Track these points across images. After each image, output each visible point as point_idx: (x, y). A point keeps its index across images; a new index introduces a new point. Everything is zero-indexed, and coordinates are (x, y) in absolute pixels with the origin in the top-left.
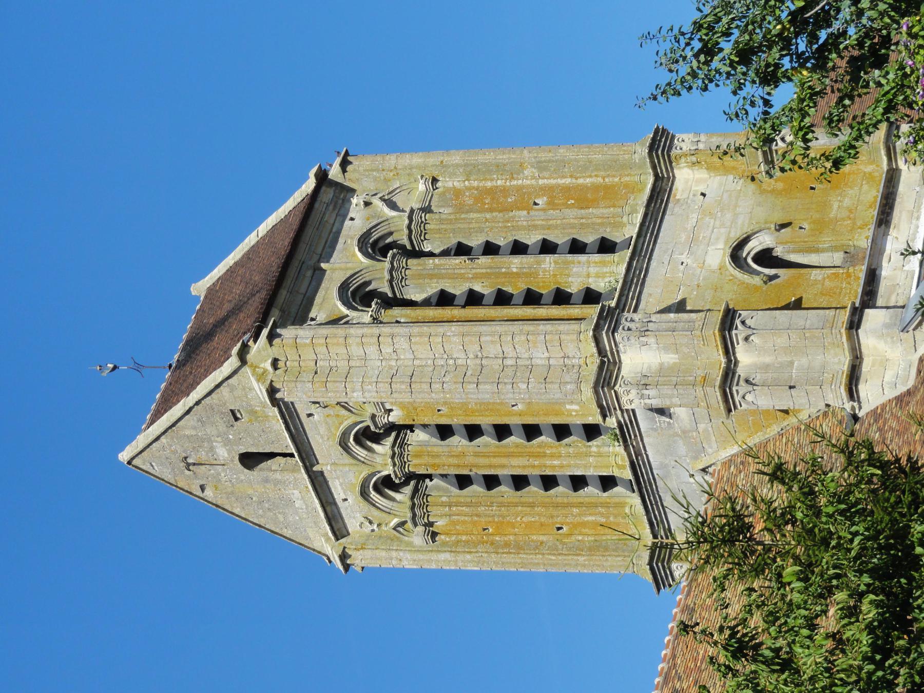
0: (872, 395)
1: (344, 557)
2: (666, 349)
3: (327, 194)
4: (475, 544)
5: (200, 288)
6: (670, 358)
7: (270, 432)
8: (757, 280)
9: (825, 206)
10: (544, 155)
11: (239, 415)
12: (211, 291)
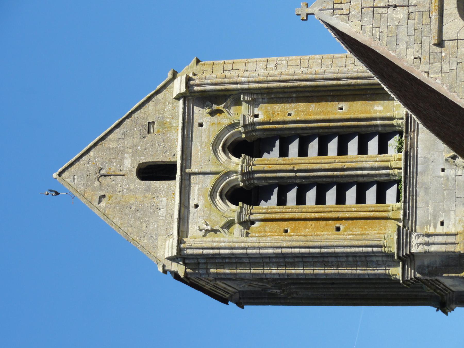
7: (168, 141)
10: (383, 249)
11: (152, 130)
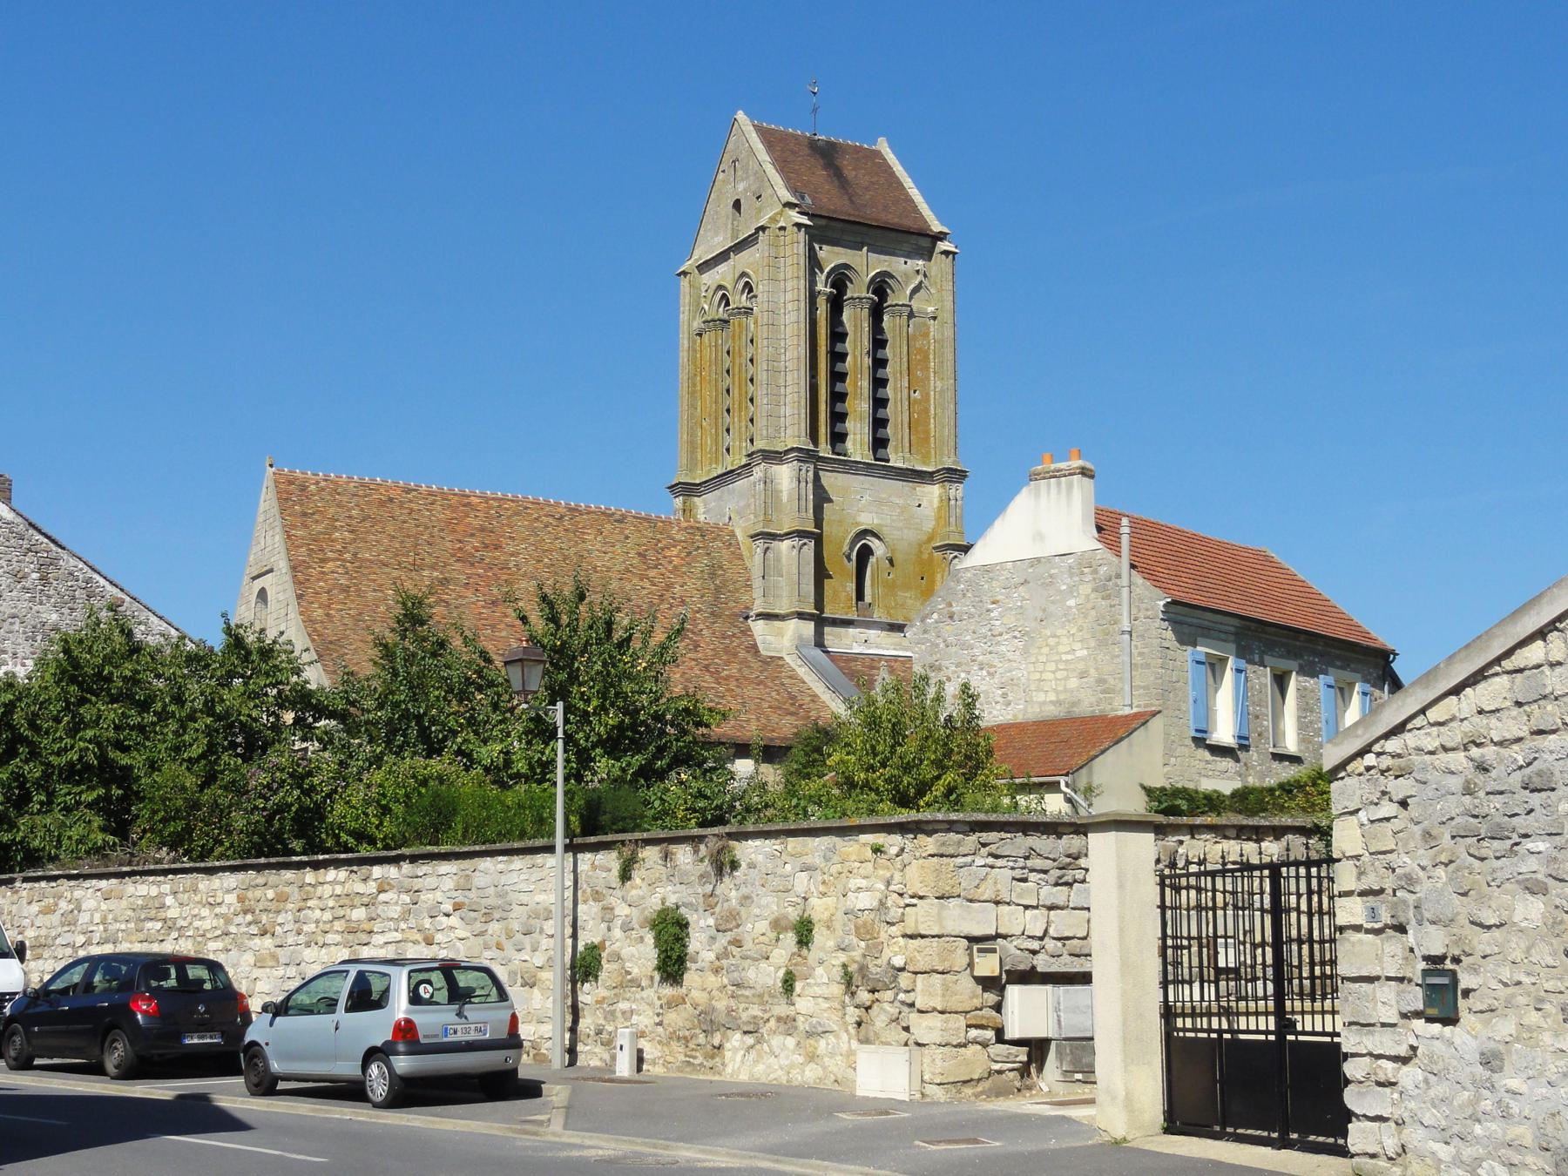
0: (759, 628)
1: (684, 273)
2: (790, 495)
3: (925, 243)
4: (694, 363)
5: (883, 146)
6: (785, 498)
8: (846, 548)
9: (907, 587)
12: (878, 154)
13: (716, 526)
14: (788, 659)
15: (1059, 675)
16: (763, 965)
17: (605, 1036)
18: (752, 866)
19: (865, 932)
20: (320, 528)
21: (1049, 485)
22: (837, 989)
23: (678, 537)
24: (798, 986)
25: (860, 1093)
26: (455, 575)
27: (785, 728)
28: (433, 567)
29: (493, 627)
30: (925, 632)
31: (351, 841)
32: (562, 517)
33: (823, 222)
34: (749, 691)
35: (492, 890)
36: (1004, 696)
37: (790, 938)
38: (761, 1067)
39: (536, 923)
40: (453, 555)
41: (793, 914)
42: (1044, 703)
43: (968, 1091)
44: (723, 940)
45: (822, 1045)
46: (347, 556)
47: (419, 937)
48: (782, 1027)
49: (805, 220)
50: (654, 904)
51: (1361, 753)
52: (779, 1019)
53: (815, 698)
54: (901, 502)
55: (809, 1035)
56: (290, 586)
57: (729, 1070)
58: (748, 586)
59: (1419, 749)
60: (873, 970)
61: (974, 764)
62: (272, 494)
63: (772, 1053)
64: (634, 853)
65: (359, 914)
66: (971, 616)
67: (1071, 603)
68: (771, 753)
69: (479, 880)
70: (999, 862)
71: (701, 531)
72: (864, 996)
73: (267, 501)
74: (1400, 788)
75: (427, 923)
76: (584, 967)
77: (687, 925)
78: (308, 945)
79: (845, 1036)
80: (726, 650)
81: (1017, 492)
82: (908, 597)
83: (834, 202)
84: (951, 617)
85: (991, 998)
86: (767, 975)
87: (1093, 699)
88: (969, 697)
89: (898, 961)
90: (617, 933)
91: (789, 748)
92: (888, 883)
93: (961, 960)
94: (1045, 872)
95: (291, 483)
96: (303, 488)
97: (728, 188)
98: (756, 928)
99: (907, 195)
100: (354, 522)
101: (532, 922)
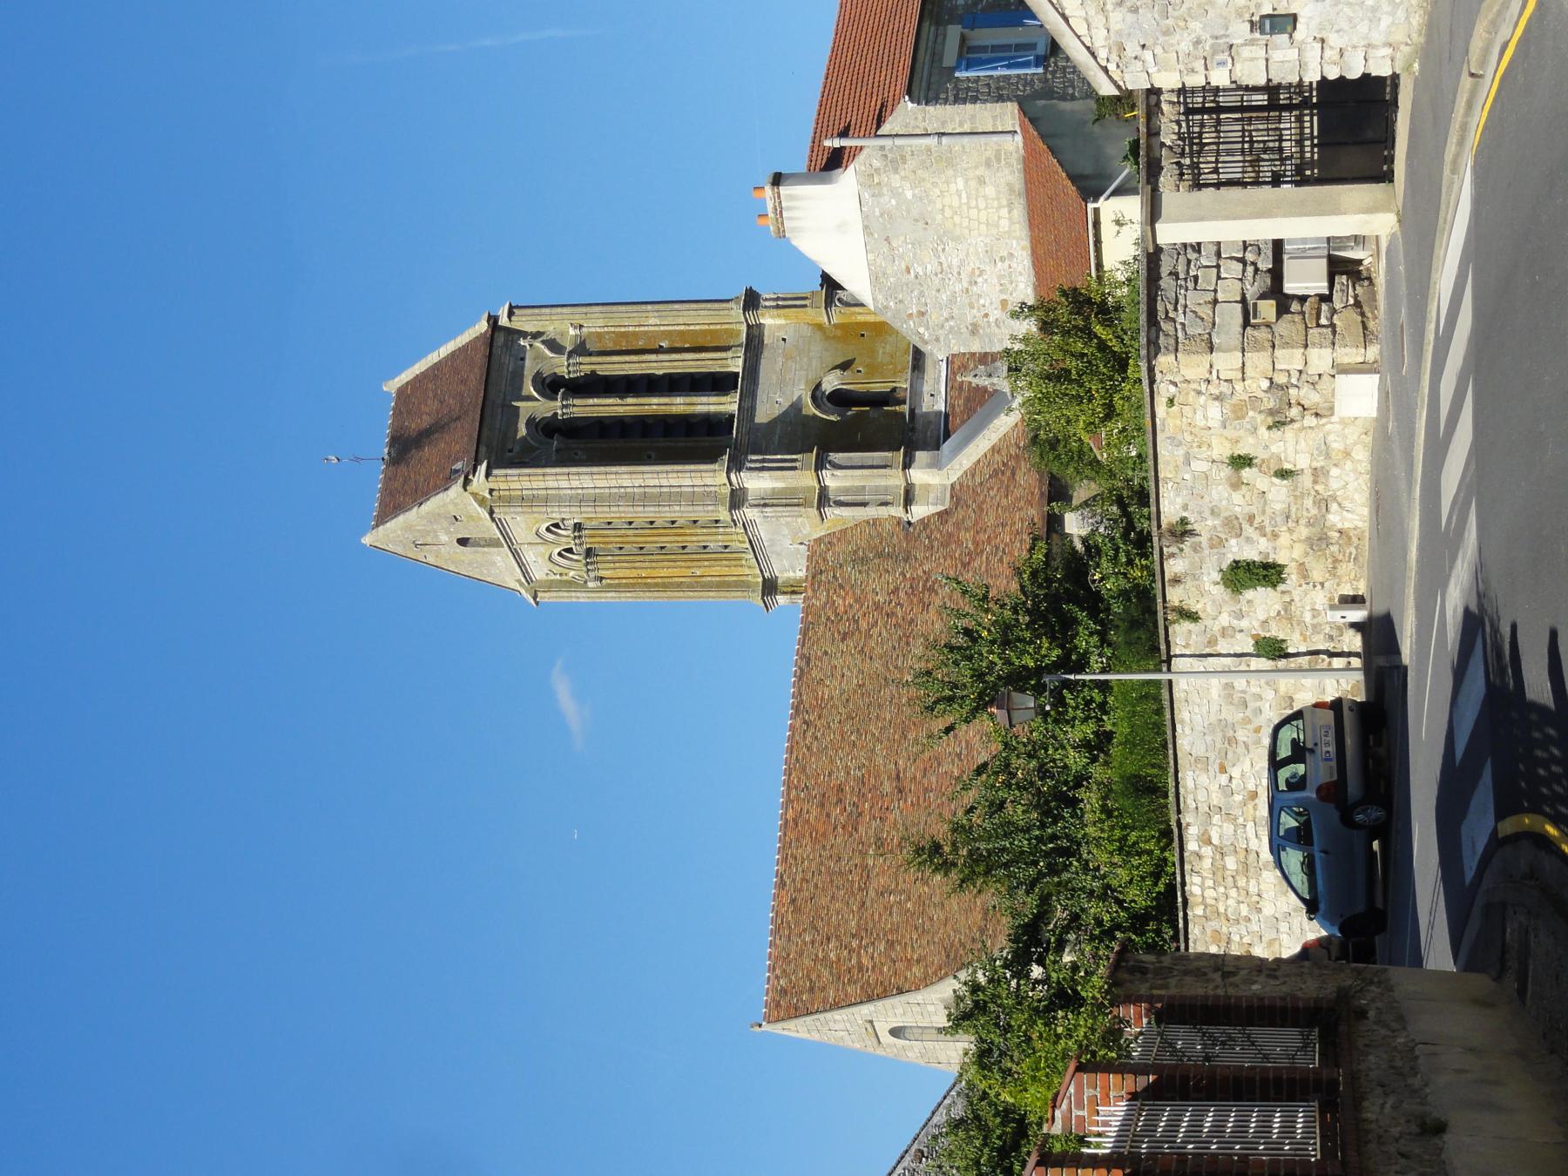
2: (777, 479)
3: (500, 339)
5: (393, 386)
6: (780, 485)
12: (401, 391)
13: (810, 558)
14: (954, 479)
15: (982, 205)
16: (1270, 496)
17: (1334, 633)
18: (1185, 507)
19: (1239, 412)
20: (826, 973)
21: (790, 219)
22: (1289, 432)
23: (823, 600)
24: (1287, 466)
25: (1374, 414)
26: (871, 832)
27: (1028, 480)
28: (864, 854)
29: (926, 790)
30: (937, 340)
31: (1164, 880)
32: (805, 722)
33: (483, 449)
34: (990, 519)
35: (1208, 738)
36: (1002, 259)
37: (1246, 473)
38: (1357, 496)
39: (1236, 696)
40: (851, 835)
41: (1227, 471)
42: (1010, 219)
43: (1371, 324)
44: (1249, 530)
45: (1336, 445)
46: (855, 944)
47: (1250, 806)
48: (1321, 479)
49: (483, 468)
50: (1219, 591)
51: (1106, 70)
52: (1315, 482)
53: (995, 450)
54: (780, 360)
55: (1328, 456)
56: (888, 1002)
57: (1360, 524)
58: (875, 523)
59: (1107, 39)
60: (1271, 405)
61: (1079, 301)
62: (791, 1024)
63: (1344, 487)
64: (1174, 609)
65: (1231, 863)
66: (922, 294)
67: (909, 194)
68: (1058, 492)
69: (1199, 750)
70: (1182, 301)
71: (815, 574)
72: (1294, 412)
73: (799, 1029)
74: (1132, 49)
75: (1238, 798)
76: (1273, 649)
77: (1236, 562)
78: (1259, 910)
79: (1329, 427)
80: (945, 545)
81: (795, 249)
82: (883, 352)
83: (463, 436)
84: (922, 314)
85: (1295, 307)
86: (1279, 492)
87: (1007, 171)
88: (1022, 311)
89: (1265, 384)
90: (1244, 624)
91: (1053, 478)
92: (1199, 393)
93: (1263, 334)
94: (1189, 262)
95: (778, 1005)
96: (784, 992)
97: (447, 554)
98: (1238, 503)
99: (447, 358)
100: (818, 938)
101: (1236, 701)
